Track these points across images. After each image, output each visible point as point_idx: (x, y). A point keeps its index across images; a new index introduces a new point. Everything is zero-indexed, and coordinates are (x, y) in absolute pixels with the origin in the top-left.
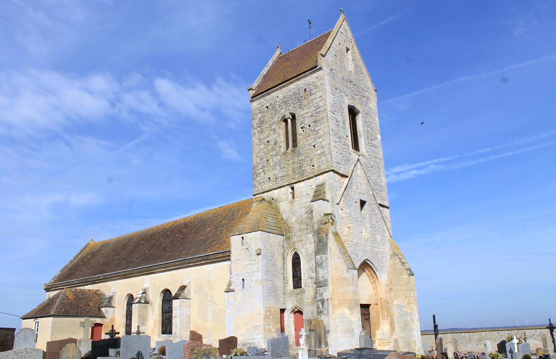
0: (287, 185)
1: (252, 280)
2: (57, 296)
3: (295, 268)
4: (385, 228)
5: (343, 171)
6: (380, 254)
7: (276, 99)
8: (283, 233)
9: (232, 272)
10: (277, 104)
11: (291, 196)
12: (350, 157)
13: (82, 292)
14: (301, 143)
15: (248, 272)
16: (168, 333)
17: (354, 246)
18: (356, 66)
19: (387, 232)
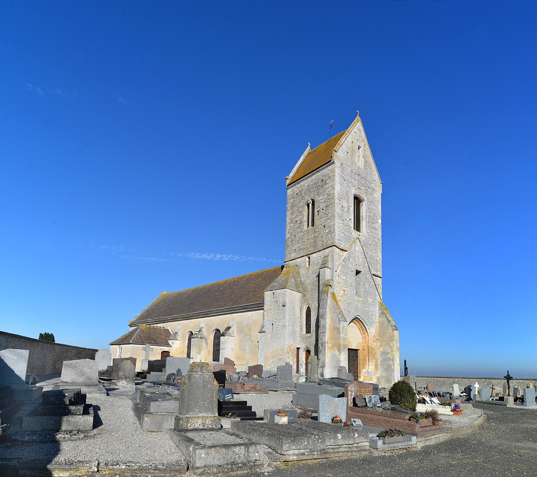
0: (306, 255)
2: (136, 330)
4: (377, 293)
5: (343, 247)
6: (370, 312)
7: (303, 187)
8: (301, 292)
9: (264, 318)
10: (303, 191)
11: (308, 263)
12: (351, 236)
13: (154, 328)
14: (317, 223)
16: (217, 360)
17: (347, 305)
18: (366, 162)
19: (378, 296)
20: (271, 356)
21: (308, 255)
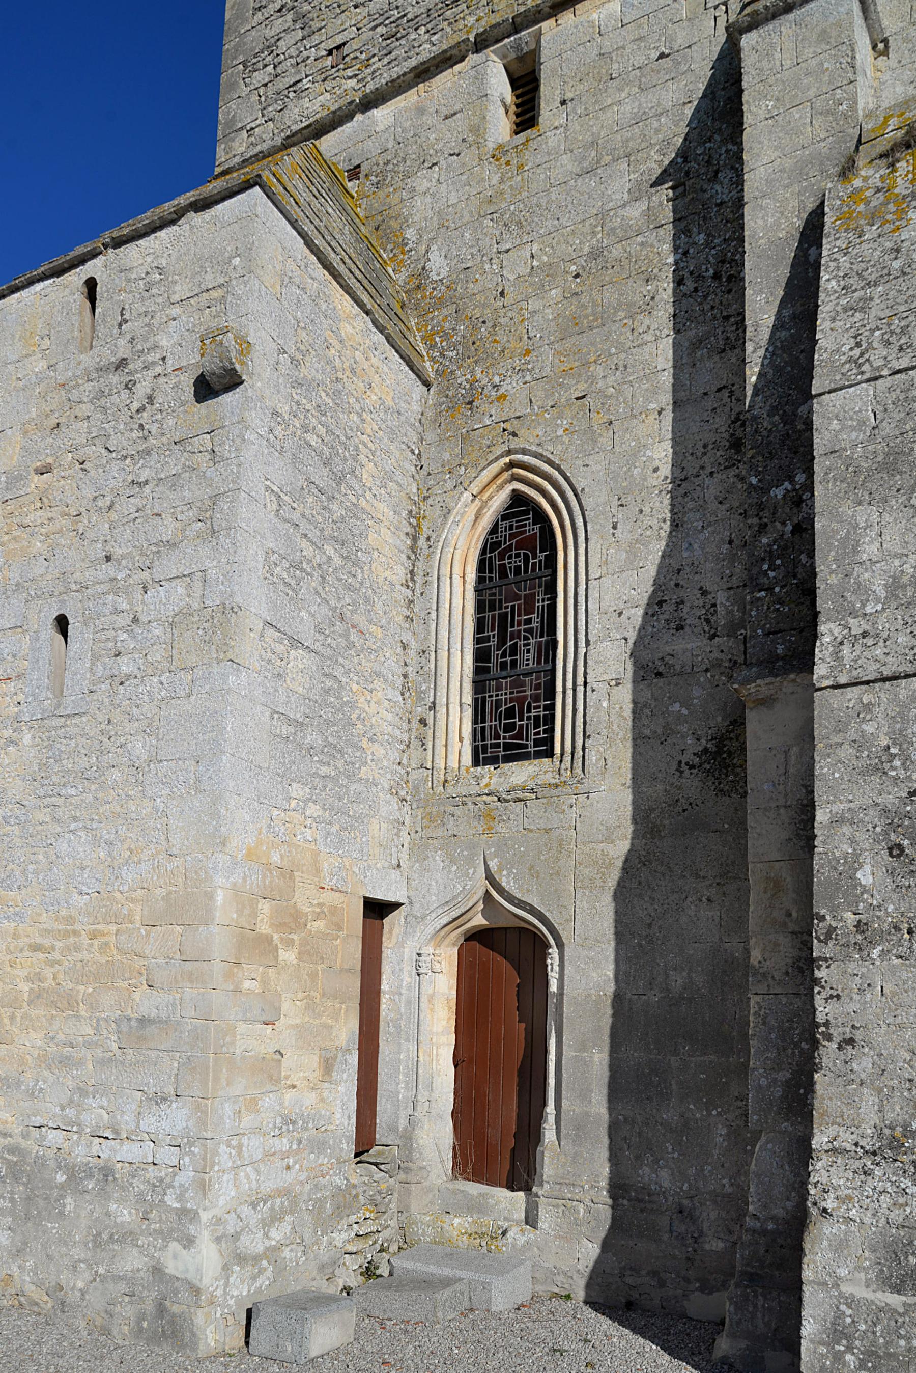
0: (481, 44)
1: (135, 620)
3: (503, 617)
15: (108, 558)
20: (25, 987)
21: (516, 26)
